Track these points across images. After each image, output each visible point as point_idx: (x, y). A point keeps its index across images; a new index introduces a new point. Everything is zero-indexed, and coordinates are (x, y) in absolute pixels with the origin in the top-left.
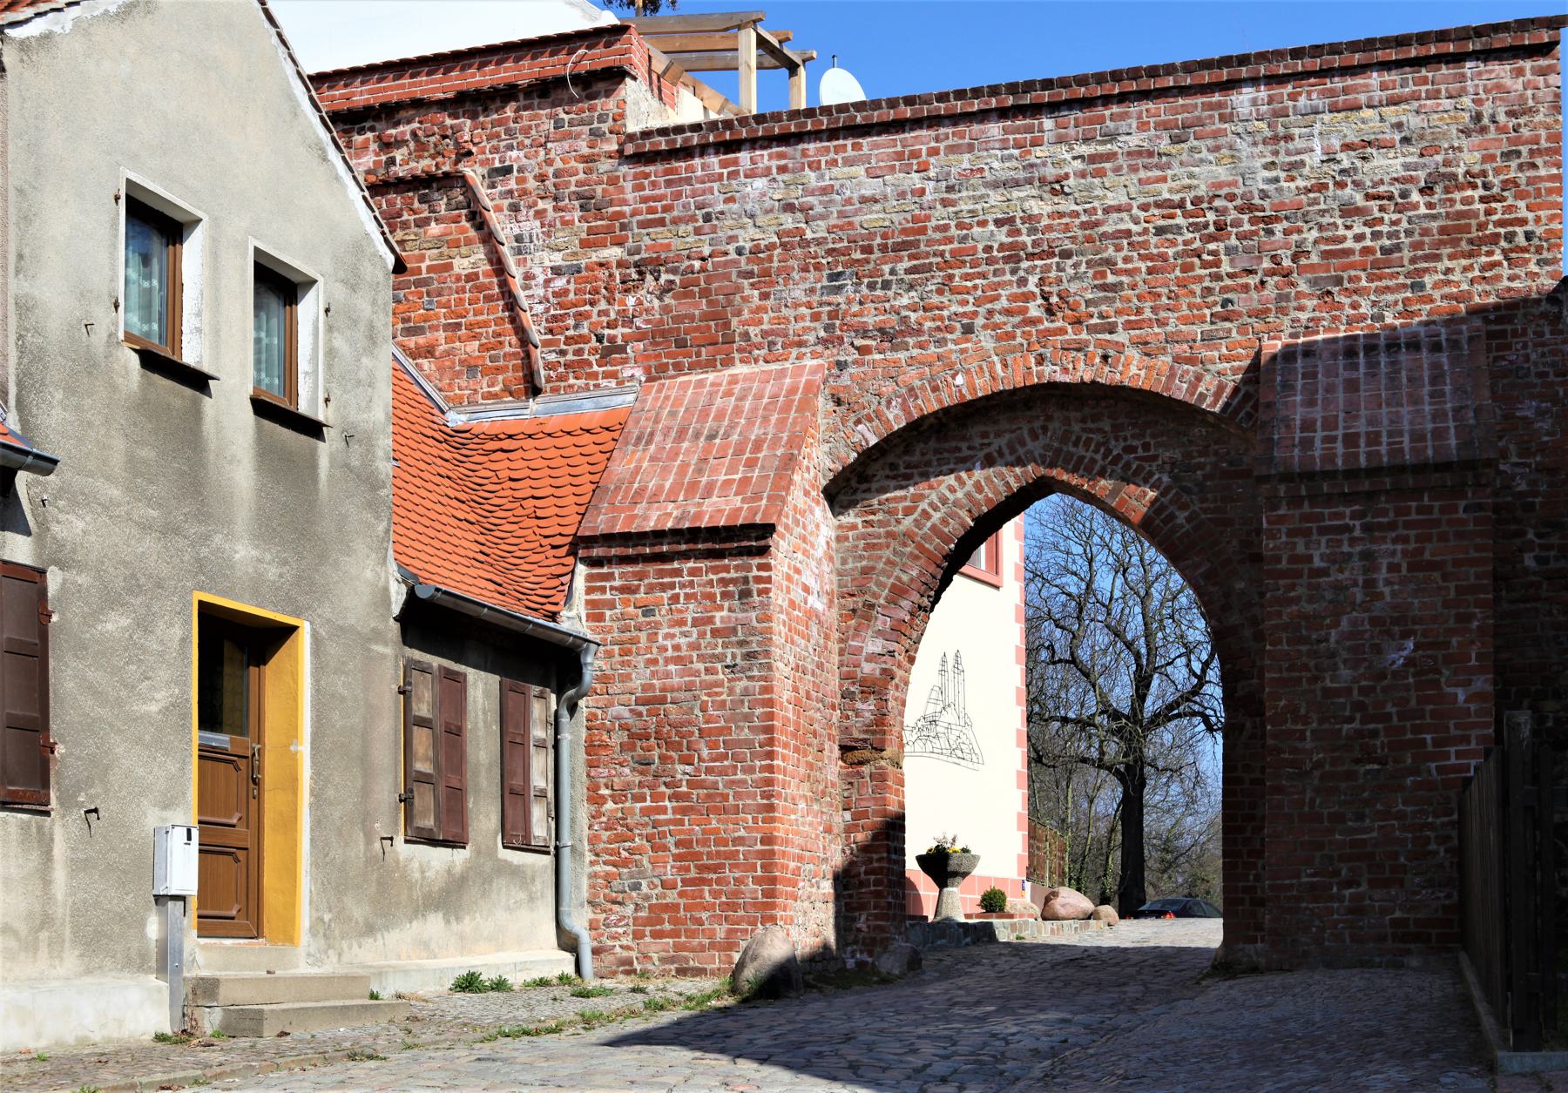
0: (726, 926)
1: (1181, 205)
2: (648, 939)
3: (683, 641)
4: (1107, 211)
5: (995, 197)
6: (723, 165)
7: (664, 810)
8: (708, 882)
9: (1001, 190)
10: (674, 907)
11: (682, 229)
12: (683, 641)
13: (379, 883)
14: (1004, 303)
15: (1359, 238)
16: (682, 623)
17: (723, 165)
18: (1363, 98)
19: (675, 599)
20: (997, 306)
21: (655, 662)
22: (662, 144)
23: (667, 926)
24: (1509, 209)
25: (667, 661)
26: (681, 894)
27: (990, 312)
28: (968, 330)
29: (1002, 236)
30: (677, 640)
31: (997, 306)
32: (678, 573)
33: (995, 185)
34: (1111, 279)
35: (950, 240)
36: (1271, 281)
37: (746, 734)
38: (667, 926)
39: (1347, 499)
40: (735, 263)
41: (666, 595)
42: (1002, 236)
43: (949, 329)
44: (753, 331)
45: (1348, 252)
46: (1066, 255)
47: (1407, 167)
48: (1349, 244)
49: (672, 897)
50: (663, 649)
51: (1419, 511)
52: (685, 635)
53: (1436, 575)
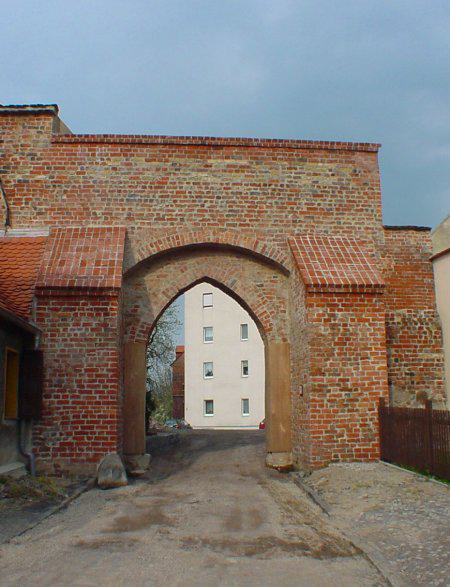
0: (93, 452)
1: (259, 185)
2: (58, 457)
3: (79, 332)
4: (234, 184)
5: (194, 174)
6: (89, 150)
7: (68, 403)
8: (87, 433)
10: (70, 444)
11: (71, 171)
12: (79, 332)
13: (137, 492)
14: (196, 212)
15: (319, 204)
16: (78, 325)
17: (89, 150)
18: (319, 159)
19: (76, 315)
20: (193, 213)
21: (66, 340)
22: (160, 140)
23: (68, 452)
24: (366, 201)
25: (71, 340)
26: (74, 438)
27: (191, 215)
30: (76, 332)
31: (193, 213)
32: (77, 304)
34: (235, 208)
35: (176, 188)
36: (290, 216)
37: (105, 372)
38: (68, 452)
39: (338, 294)
40: (93, 186)
41: (72, 313)
43: (176, 219)
44: (98, 212)
45: (315, 209)
46: (219, 198)
47: (334, 183)
48: (315, 206)
49: (70, 439)
50: (69, 335)
51: (361, 300)
52: (79, 330)
53: (367, 324)
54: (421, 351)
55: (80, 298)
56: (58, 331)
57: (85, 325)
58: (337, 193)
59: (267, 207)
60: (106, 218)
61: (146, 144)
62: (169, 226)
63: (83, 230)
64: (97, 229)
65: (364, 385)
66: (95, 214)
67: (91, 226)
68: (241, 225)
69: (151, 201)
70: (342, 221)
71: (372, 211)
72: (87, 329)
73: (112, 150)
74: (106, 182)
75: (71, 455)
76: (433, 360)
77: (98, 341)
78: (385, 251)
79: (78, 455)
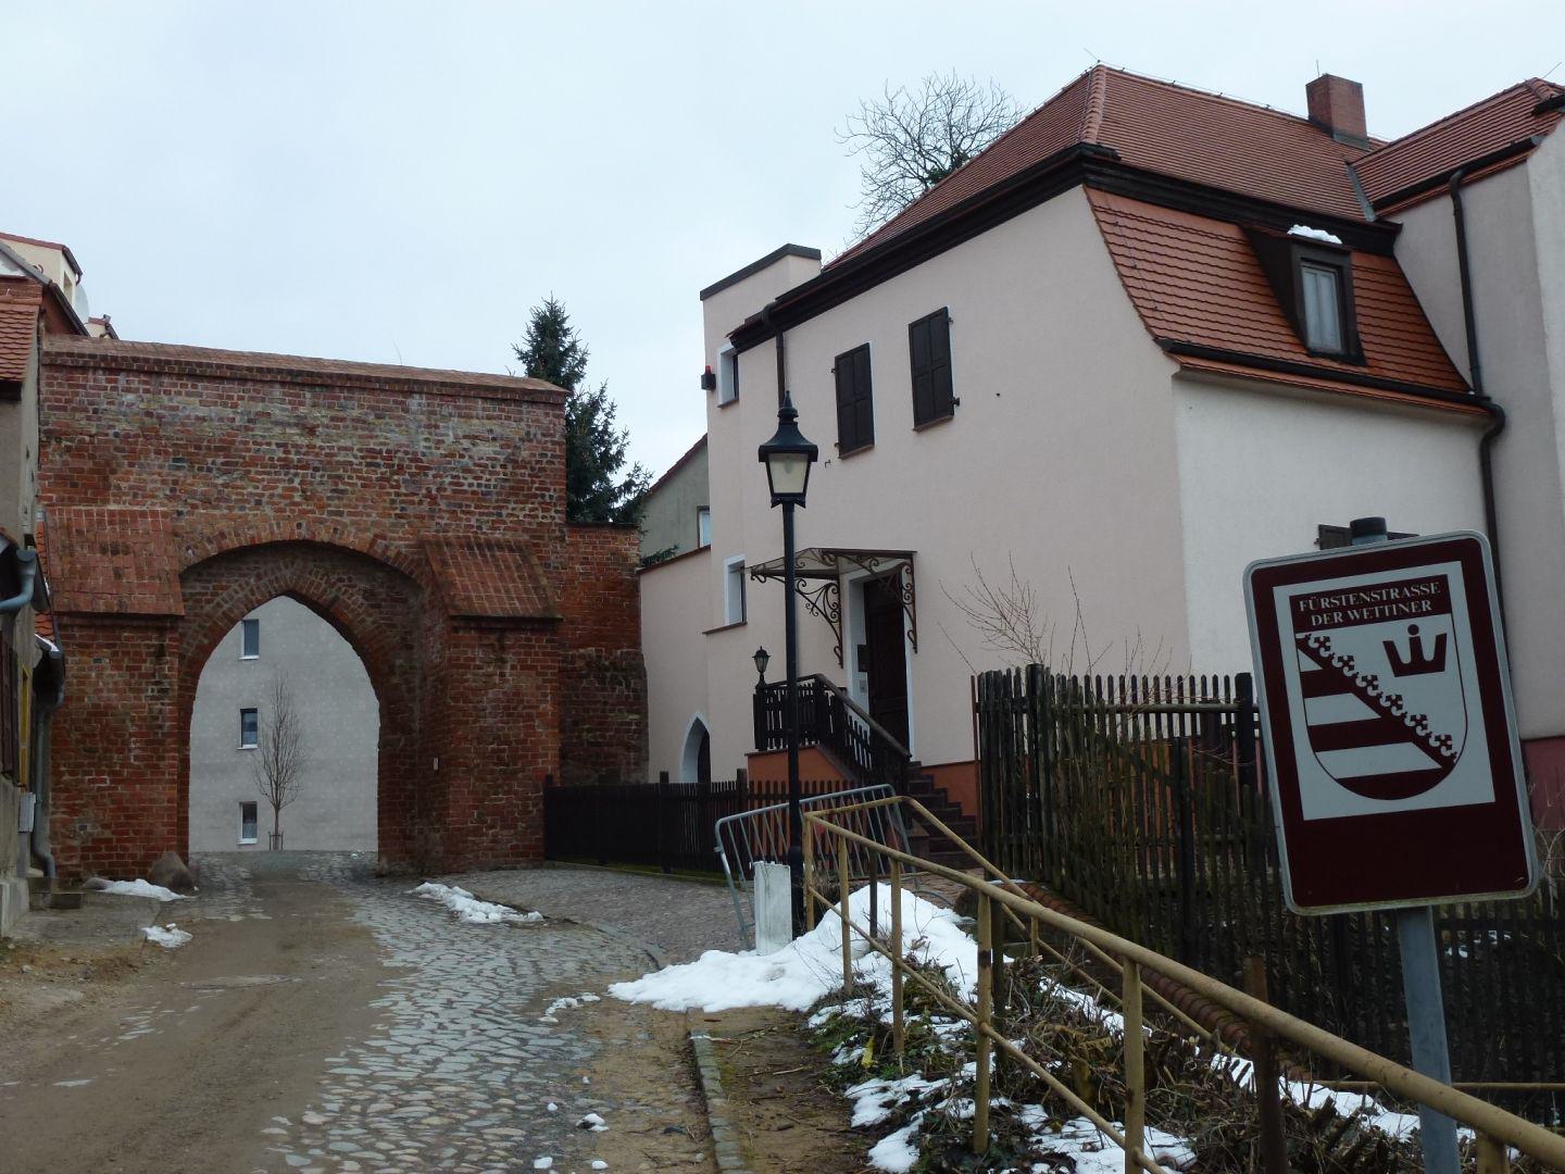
4: (339, 449)
5: (278, 430)
6: (109, 381)
9: (143, 378)
10: (108, 841)
11: (77, 415)
15: (471, 485)
28: (259, 503)
29: (280, 454)
33: (277, 423)
34: (341, 487)
42: (280, 454)
45: (465, 492)
47: (495, 452)
48: (466, 488)
50: (106, 684)
54: (612, 711)
55: (123, 628)
56: (89, 677)
57: (129, 668)
58: (498, 469)
59: (392, 487)
60: (135, 495)
61: (202, 377)
62: (237, 512)
63: (100, 514)
64: (122, 513)
65: (526, 756)
66: (119, 487)
67: (113, 507)
68: (350, 514)
69: (210, 470)
70: (504, 512)
71: (551, 497)
72: (132, 676)
73: (145, 383)
74: (137, 436)
75: (110, 856)
76: (629, 724)
77: (149, 693)
78: (1009, 671)
79: (119, 856)
